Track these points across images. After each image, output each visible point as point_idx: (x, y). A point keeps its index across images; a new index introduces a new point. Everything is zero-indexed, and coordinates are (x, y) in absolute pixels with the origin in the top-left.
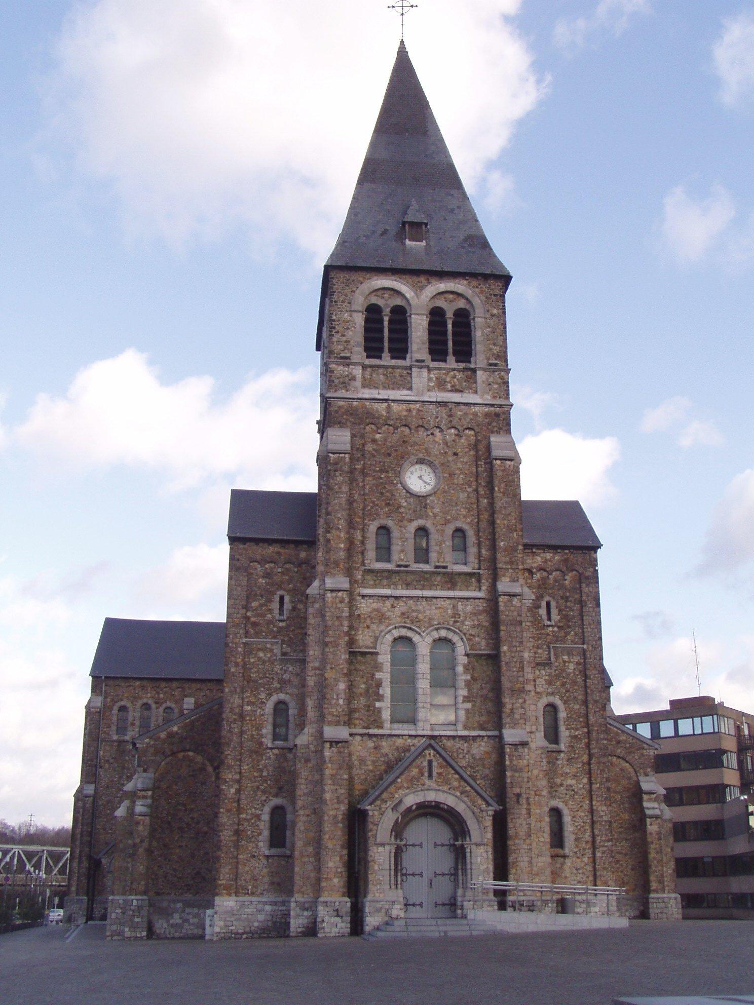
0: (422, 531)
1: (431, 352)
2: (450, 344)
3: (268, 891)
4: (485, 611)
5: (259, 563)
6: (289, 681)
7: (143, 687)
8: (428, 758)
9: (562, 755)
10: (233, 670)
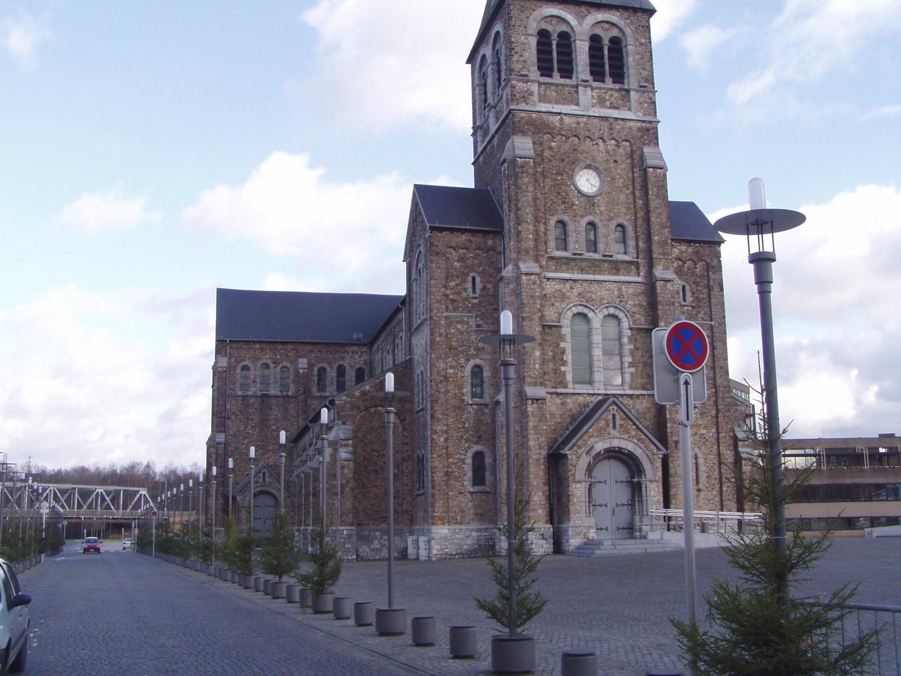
0: (592, 224)
1: (592, 73)
2: (607, 67)
3: (473, 520)
4: (643, 293)
5: (454, 249)
6: (483, 348)
7: (262, 350)
8: (612, 412)
10: (438, 339)
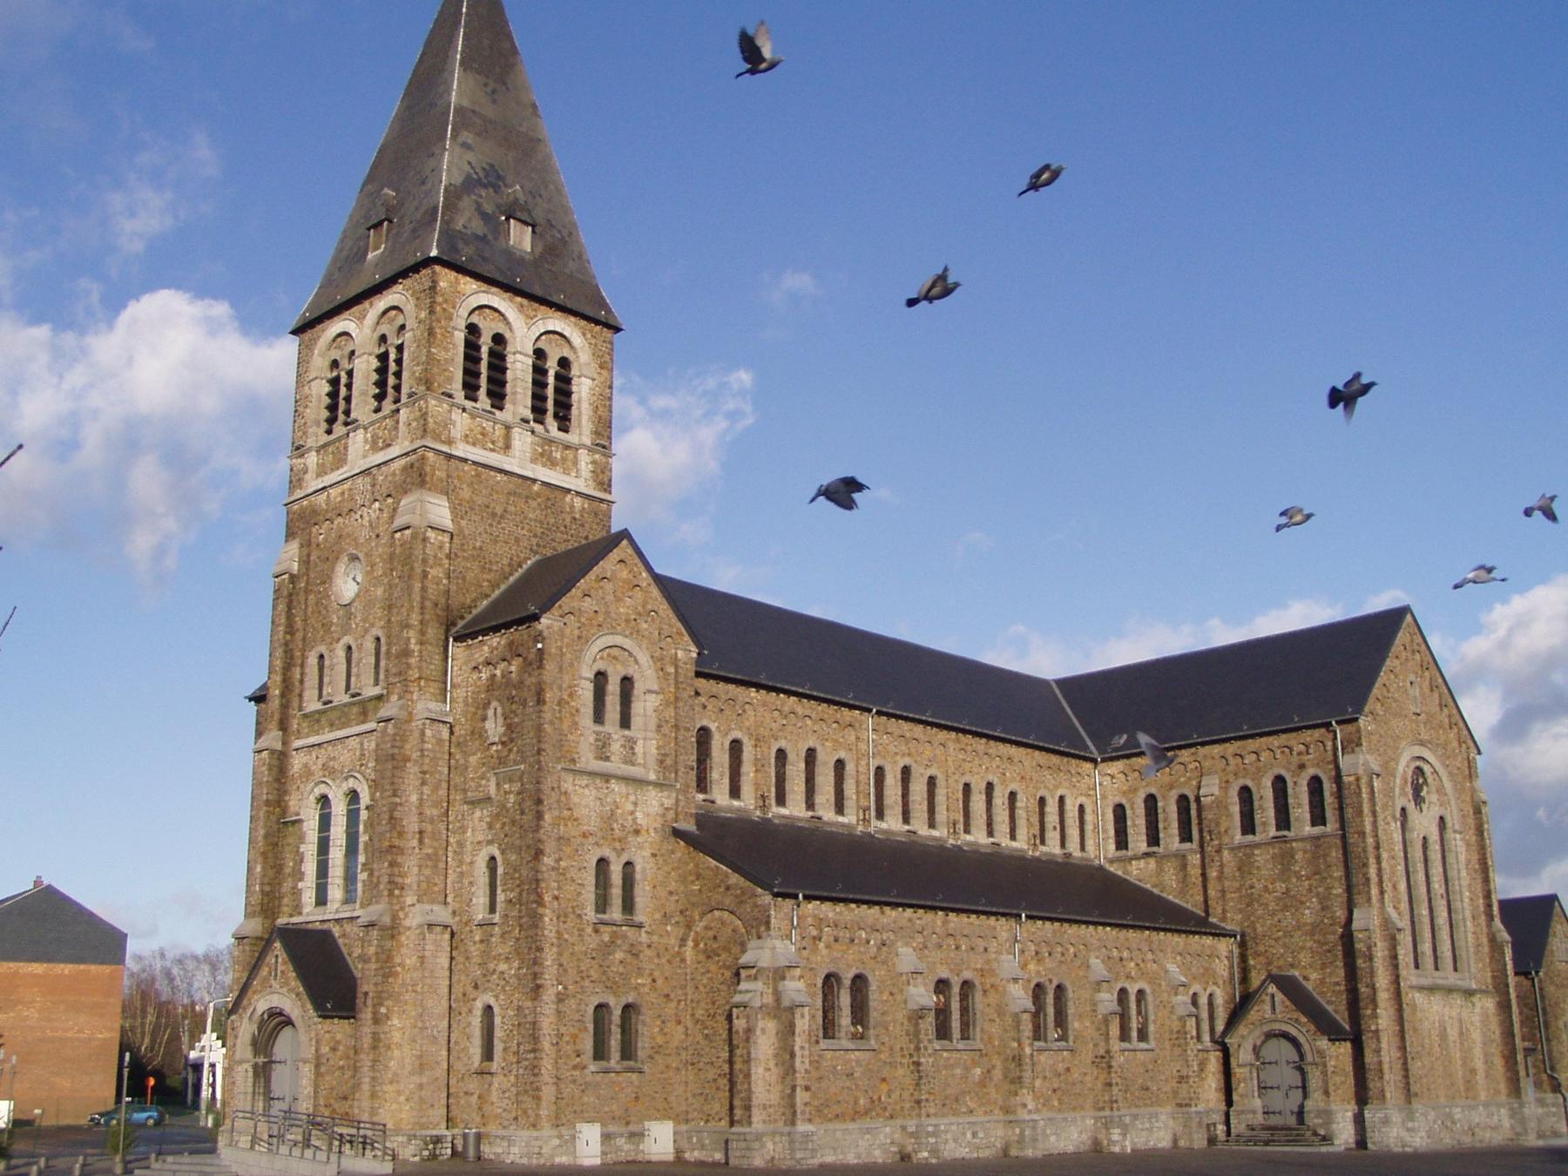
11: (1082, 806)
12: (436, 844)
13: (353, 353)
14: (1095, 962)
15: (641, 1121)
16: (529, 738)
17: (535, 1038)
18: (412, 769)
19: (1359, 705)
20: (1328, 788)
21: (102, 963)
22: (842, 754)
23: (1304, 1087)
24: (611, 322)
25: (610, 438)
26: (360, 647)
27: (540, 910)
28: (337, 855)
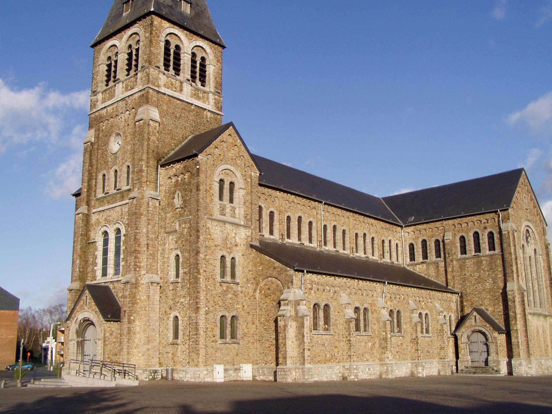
9: (179, 284)
11: (396, 243)
12: (154, 249)
13: (117, 53)
14: (411, 302)
15: (239, 364)
16: (193, 205)
17: (197, 329)
18: (144, 218)
19: (508, 204)
20: (496, 236)
21: (11, 310)
22: (311, 219)
23: (488, 352)
24: (222, 44)
25: (221, 90)
26: (121, 170)
27: (199, 276)
28: (111, 255)
